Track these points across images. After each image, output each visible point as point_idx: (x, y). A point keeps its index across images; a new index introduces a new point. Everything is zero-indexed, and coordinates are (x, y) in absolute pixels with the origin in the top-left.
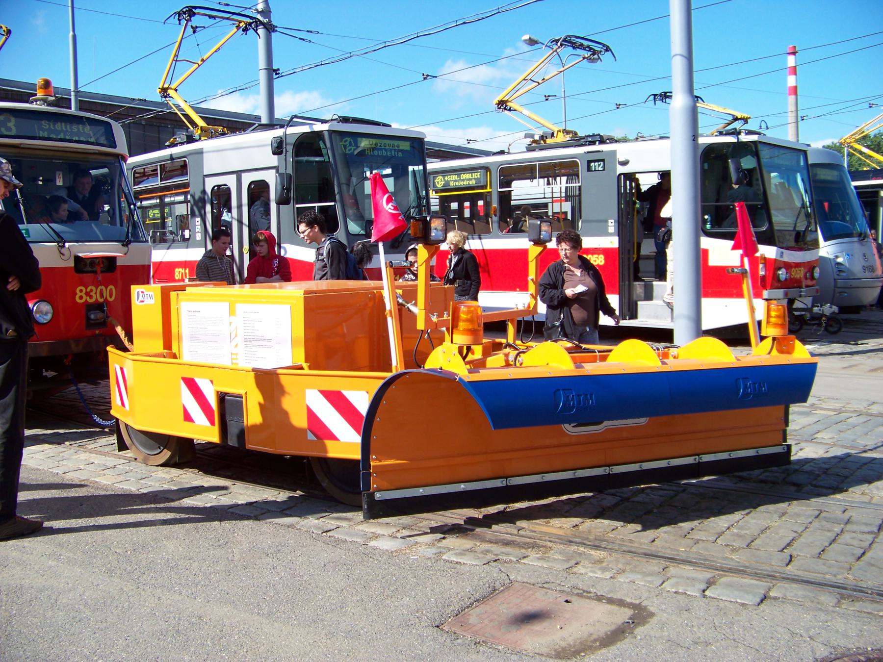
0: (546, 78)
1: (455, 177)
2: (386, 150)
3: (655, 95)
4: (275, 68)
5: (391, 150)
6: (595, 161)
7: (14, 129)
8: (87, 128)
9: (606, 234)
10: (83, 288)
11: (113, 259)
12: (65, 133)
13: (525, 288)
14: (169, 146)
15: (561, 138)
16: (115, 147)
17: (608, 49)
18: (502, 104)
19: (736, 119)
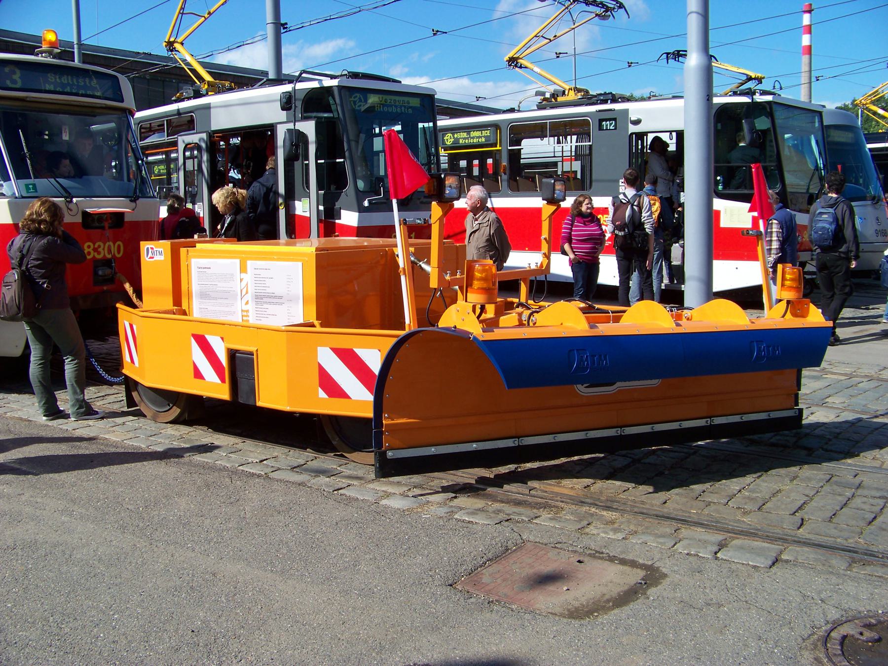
2: (396, 107)
3: (668, 54)
4: (282, 22)
5: (401, 107)
6: (606, 120)
11: (121, 215)
15: (572, 96)
16: (122, 101)
19: (750, 79)
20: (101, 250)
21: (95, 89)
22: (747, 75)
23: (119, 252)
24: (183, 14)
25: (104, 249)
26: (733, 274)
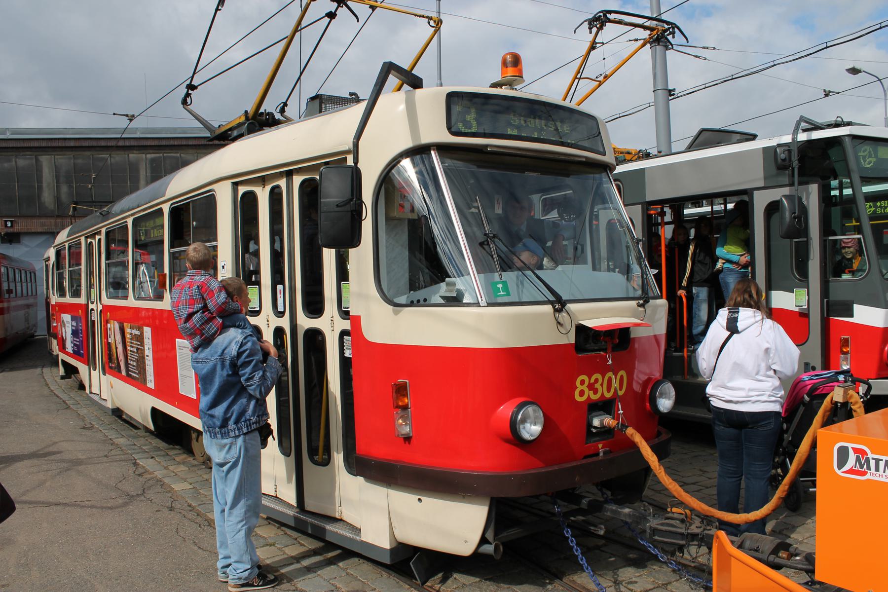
4: (670, 88)
7: (474, 123)
10: (584, 377)
20: (597, 386)
23: (621, 389)
24: (580, 79)
25: (602, 385)
26: (615, 384)
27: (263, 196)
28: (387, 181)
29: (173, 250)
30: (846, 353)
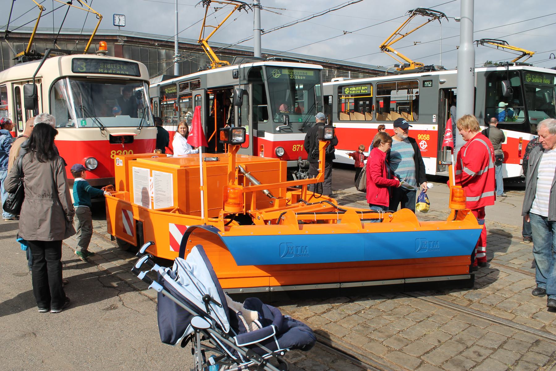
0: (408, 32)
1: (354, 89)
3: (478, 41)
6: (427, 81)
7: (85, 68)
8: (125, 67)
9: (430, 122)
10: (115, 151)
11: (131, 137)
12: (104, 69)
13: (508, 138)
14: (199, 71)
15: (412, 67)
16: (140, 76)
17: (443, 15)
18: (383, 48)
19: (525, 54)
21: (109, 69)
22: (523, 52)
27: (21, 88)
28: (54, 88)
29: (264, 68)
30: (262, 151)
